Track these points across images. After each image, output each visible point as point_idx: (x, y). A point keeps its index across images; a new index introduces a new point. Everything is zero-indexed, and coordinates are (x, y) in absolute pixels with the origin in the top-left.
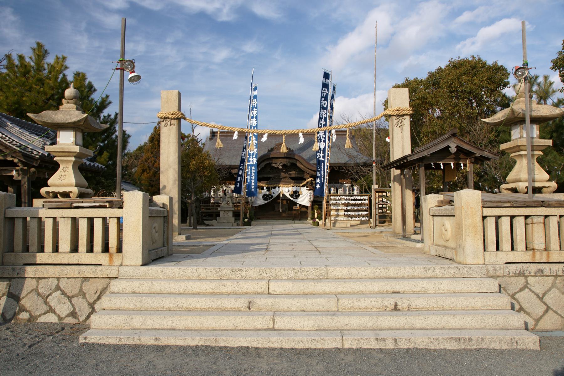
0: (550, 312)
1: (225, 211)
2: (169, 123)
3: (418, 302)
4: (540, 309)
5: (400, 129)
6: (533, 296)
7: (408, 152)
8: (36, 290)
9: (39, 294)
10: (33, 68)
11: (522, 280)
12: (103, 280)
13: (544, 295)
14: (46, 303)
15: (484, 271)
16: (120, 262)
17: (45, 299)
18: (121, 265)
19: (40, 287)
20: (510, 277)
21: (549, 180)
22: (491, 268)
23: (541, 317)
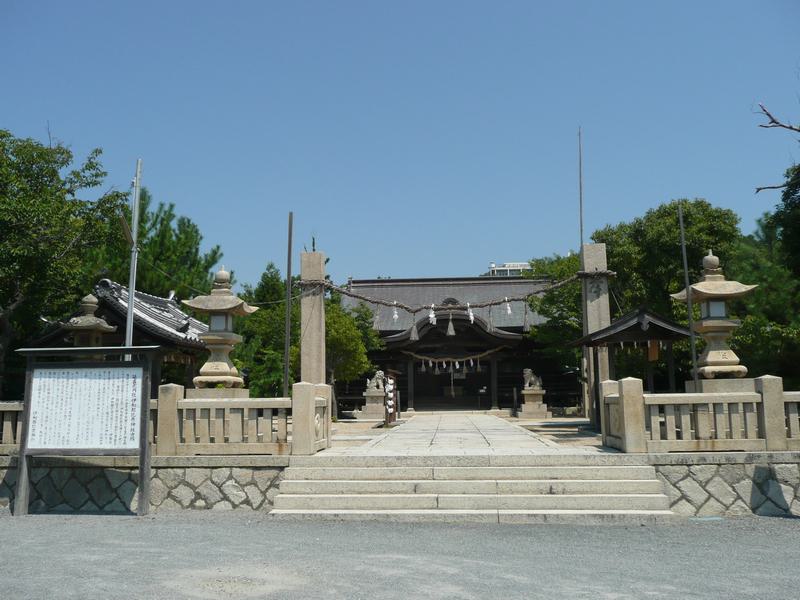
7: (606, 324)
9: (213, 482)
10: (174, 231)
22: (653, 458)
23: (702, 505)
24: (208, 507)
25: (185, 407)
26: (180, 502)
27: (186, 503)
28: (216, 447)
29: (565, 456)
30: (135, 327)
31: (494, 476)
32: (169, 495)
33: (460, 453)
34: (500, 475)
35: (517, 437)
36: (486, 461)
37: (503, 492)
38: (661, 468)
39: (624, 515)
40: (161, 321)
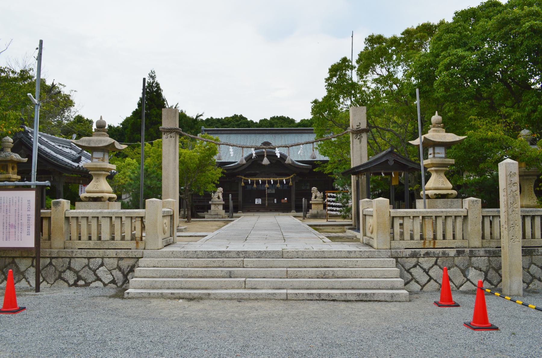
0: (432, 281)
1: (215, 204)
2: (169, 135)
3: (339, 271)
4: (426, 278)
5: (359, 140)
6: (421, 271)
8: (88, 265)
9: (90, 268)
11: (414, 260)
12: (132, 259)
13: (429, 269)
14: (96, 275)
15: (389, 254)
16: (143, 247)
17: (94, 271)
18: (145, 249)
19: (90, 263)
20: (407, 258)
21: (452, 189)
24: (87, 284)
25: (70, 216)
26: (67, 282)
27: (71, 282)
28: (91, 244)
29: (335, 251)
30: (39, 156)
31: (285, 266)
32: (60, 278)
33: (263, 248)
34: (290, 265)
35: (304, 235)
36: (281, 255)
37: (291, 278)
38: (399, 259)
39: (374, 294)
40: (61, 154)
